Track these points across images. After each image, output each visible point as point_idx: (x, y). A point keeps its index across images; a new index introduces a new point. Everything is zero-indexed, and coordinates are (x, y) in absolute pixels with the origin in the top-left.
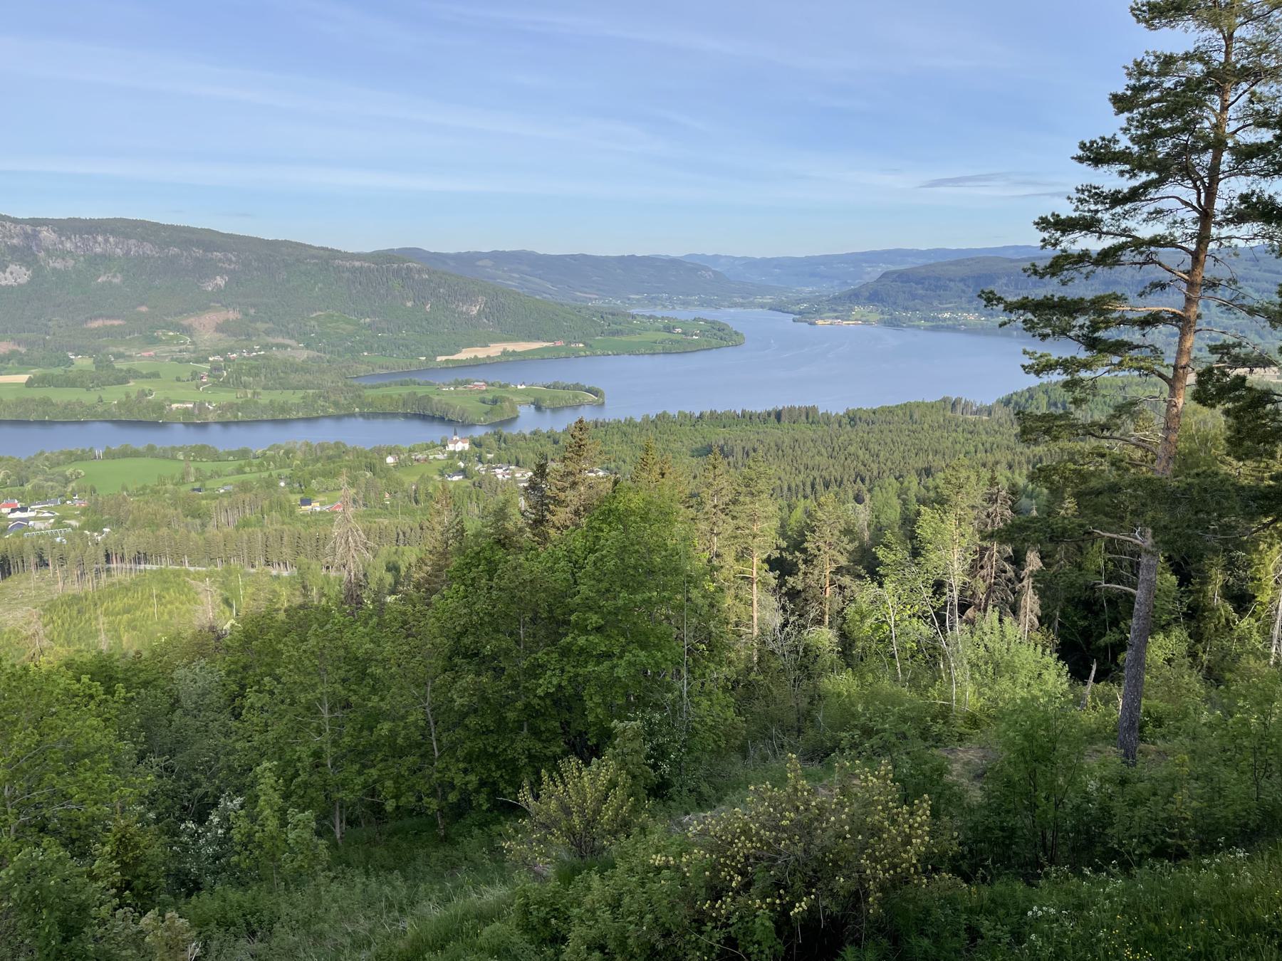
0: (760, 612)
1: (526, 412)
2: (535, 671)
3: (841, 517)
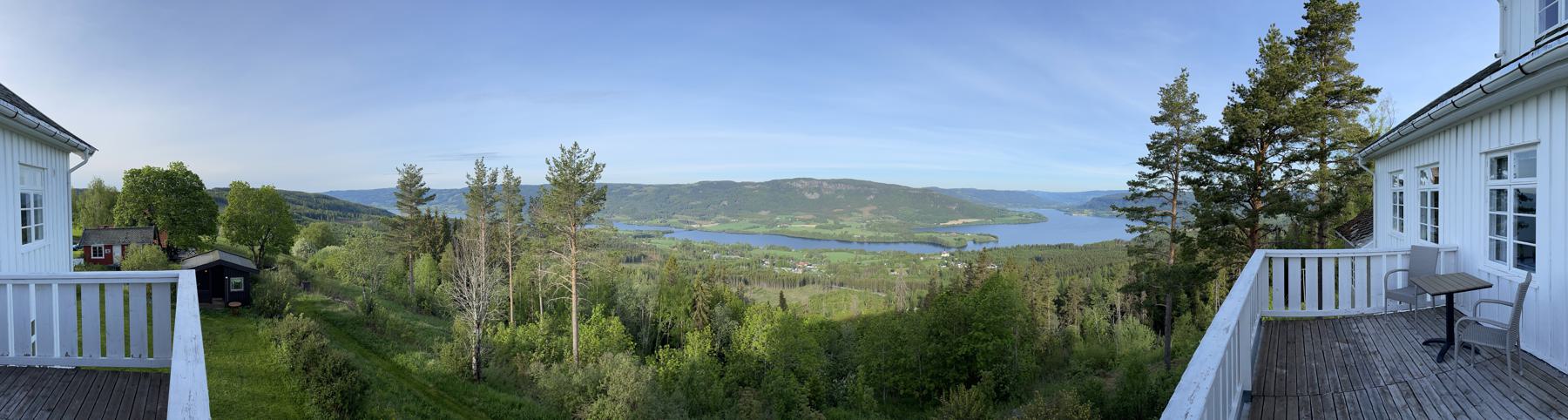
0: (1051, 321)
1: (970, 244)
2: (958, 344)
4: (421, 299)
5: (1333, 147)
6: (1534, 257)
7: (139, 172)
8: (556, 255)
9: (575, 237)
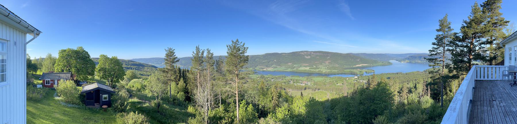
2: (371, 106)
3: (407, 86)
4: (174, 100)
5: (494, 40)
6: (27, 99)
7: (65, 51)
8: (230, 82)
9: (237, 75)
